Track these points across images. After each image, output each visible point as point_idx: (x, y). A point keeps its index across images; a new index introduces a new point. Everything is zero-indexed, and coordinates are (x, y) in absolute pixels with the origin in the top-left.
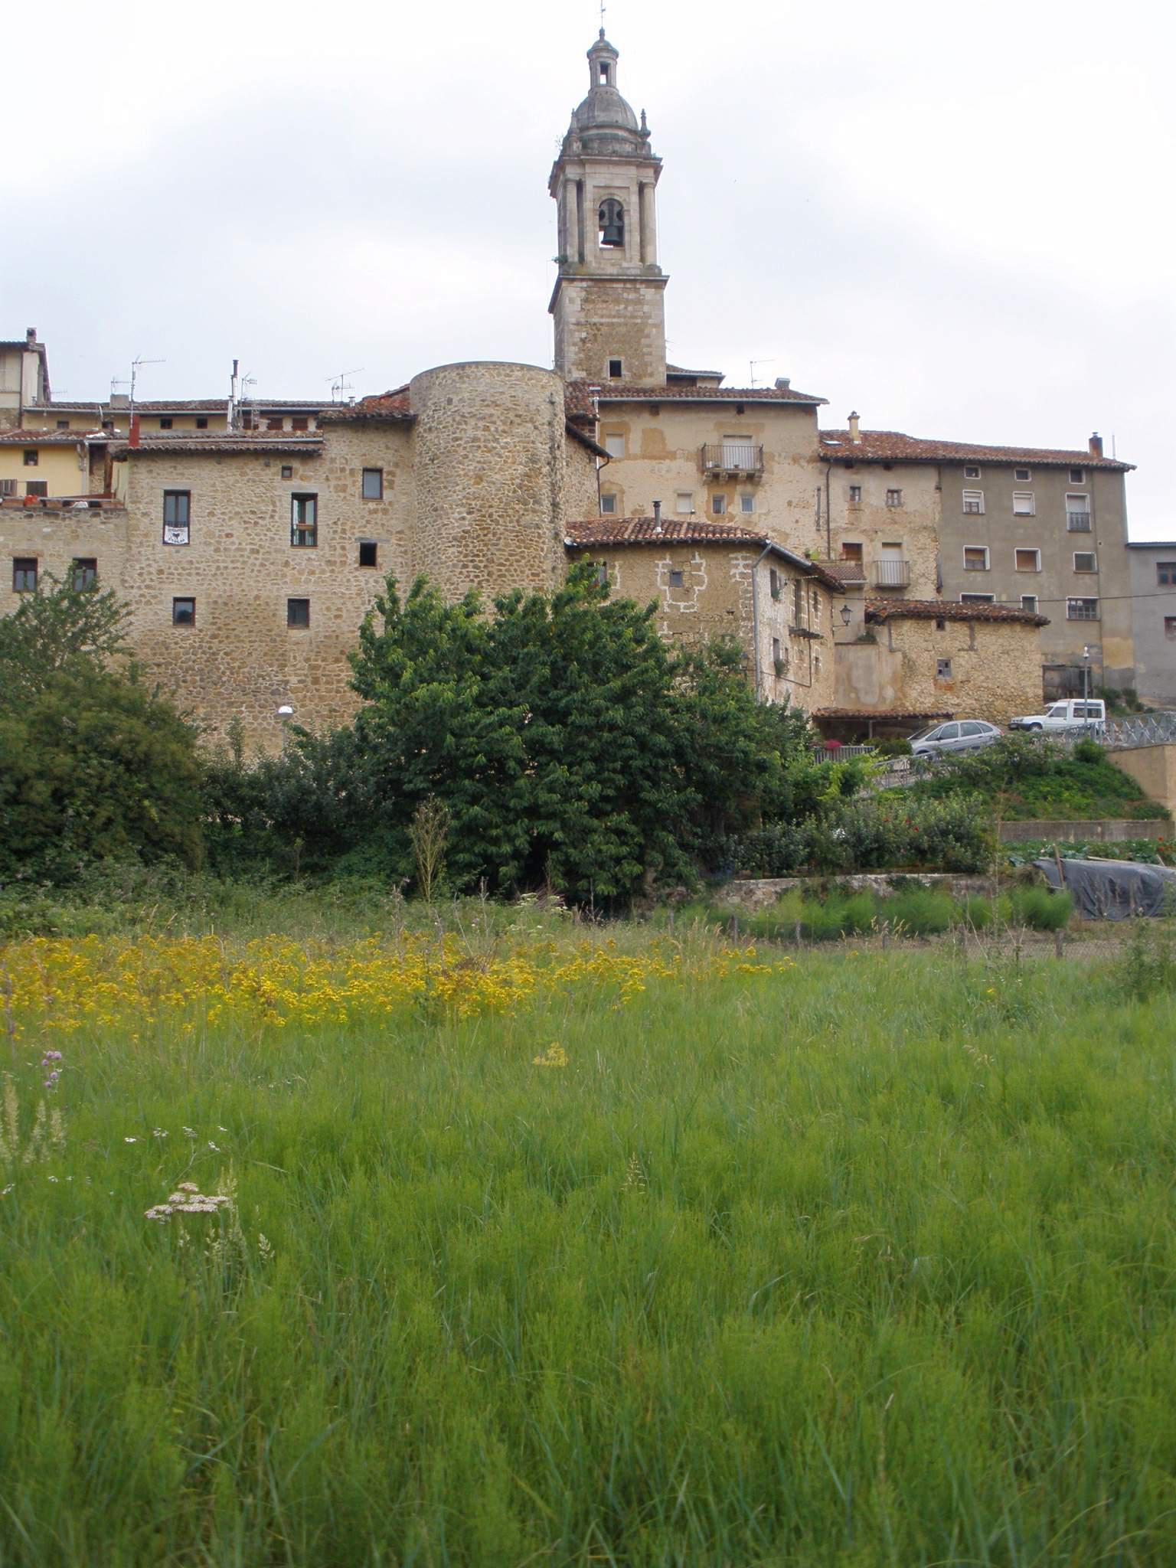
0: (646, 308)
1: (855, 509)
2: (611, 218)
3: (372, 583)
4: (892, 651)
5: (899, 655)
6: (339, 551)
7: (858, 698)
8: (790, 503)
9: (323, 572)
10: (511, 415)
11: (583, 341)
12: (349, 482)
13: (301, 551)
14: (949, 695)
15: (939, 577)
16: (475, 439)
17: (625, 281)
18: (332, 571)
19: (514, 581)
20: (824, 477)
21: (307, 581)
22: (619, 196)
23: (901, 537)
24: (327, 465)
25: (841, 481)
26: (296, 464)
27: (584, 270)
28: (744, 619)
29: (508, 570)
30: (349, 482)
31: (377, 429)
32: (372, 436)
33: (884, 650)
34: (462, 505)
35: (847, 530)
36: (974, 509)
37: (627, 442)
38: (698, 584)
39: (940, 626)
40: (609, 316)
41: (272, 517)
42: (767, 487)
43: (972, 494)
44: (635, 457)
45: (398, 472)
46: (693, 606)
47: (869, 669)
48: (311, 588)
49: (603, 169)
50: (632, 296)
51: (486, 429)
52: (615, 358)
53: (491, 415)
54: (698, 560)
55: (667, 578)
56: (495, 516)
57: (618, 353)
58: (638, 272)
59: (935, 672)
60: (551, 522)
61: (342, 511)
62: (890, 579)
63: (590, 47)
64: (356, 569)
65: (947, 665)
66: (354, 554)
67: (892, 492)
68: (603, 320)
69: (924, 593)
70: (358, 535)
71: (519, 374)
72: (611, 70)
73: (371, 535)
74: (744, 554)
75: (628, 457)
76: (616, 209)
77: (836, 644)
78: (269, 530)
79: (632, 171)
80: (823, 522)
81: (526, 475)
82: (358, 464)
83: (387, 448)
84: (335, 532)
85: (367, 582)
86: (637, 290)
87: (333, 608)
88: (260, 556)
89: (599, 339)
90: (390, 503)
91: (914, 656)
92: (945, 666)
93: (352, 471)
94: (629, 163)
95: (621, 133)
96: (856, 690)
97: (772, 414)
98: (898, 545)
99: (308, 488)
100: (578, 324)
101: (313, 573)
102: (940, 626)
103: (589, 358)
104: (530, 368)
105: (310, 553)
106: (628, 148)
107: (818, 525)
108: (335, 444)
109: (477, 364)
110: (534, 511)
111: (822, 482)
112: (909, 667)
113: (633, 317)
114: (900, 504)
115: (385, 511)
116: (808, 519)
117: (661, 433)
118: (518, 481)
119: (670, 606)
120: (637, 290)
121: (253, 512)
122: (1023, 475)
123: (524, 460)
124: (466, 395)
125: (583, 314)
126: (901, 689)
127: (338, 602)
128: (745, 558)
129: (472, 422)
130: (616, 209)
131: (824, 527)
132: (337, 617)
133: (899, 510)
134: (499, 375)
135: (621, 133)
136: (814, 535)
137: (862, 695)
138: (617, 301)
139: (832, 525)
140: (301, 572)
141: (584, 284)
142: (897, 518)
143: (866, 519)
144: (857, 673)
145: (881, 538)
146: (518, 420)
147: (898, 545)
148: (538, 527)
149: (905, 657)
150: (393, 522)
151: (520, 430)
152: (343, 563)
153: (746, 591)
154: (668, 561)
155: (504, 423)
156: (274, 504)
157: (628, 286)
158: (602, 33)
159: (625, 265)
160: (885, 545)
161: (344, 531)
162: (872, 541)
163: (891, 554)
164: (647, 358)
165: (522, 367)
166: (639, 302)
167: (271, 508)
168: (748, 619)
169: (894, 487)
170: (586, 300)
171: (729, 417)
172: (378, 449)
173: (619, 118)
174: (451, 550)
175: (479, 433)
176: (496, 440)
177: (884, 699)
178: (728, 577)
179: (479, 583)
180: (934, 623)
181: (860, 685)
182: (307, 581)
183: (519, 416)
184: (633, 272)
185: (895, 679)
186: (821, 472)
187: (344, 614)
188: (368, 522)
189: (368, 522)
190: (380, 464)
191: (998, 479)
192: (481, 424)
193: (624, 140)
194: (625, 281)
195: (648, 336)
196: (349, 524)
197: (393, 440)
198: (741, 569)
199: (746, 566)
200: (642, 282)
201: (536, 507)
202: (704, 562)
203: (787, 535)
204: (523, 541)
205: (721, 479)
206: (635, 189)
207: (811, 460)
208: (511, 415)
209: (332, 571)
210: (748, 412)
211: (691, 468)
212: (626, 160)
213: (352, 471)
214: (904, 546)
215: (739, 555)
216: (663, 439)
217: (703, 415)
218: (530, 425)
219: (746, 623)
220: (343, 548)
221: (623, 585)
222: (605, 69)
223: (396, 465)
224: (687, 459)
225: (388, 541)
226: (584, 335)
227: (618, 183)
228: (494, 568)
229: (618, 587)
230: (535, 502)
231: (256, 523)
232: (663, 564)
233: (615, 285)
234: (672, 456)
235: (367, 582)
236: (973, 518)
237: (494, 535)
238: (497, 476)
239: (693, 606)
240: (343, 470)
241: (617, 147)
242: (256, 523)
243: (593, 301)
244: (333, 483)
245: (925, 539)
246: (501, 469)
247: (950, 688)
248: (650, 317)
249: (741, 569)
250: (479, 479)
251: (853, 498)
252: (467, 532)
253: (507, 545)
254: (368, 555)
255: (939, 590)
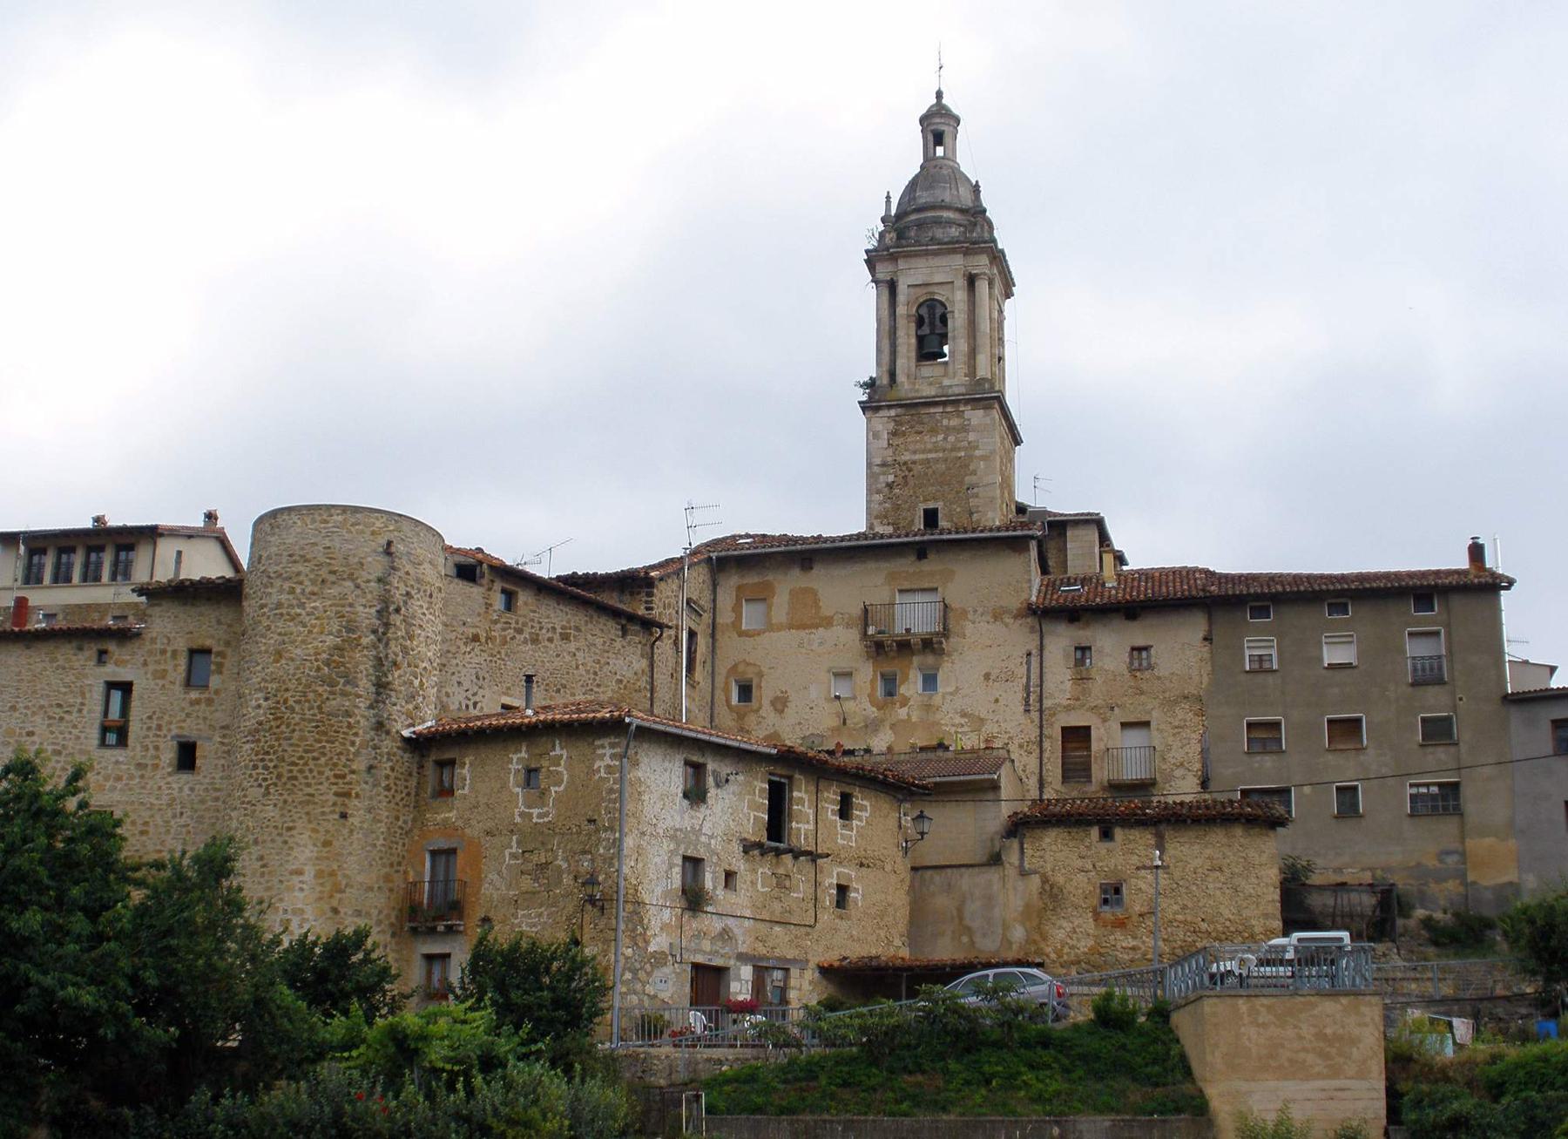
0: (972, 437)
1: (1082, 678)
2: (932, 324)
3: (186, 790)
4: (1023, 873)
5: (1036, 880)
6: (152, 752)
7: (973, 943)
8: (987, 676)
9: (131, 777)
10: (324, 573)
11: (890, 486)
12: (169, 667)
13: (108, 753)
14: (1118, 934)
15: (1205, 765)
16: (279, 605)
17: (944, 404)
18: (142, 777)
19: (308, 785)
20: (1036, 637)
21: (113, 789)
22: (941, 295)
23: (1149, 713)
24: (148, 646)
25: (1061, 640)
26: (112, 647)
27: (894, 394)
28: (606, 830)
29: (301, 771)
30: (169, 667)
31: (209, 599)
32: (203, 609)
33: (1011, 872)
34: (260, 690)
35: (1068, 709)
36: (1266, 665)
37: (770, 608)
38: (556, 785)
39: (1106, 835)
40: (923, 452)
41: (80, 711)
42: (955, 656)
43: (1259, 644)
44: (780, 628)
45: (229, 651)
46: (546, 814)
47: (989, 900)
48: (116, 796)
49: (920, 263)
50: (955, 422)
51: (292, 591)
52: (931, 505)
53: (299, 574)
54: (558, 751)
55: (522, 776)
56: (291, 702)
57: (935, 499)
58: (963, 390)
59: (1095, 901)
60: (371, 707)
61: (161, 702)
62: (1132, 771)
63: (924, 111)
64: (170, 774)
65: (1117, 891)
66: (169, 755)
67: (1140, 649)
68: (917, 457)
69: (1183, 789)
70: (175, 732)
71: (340, 518)
72: (947, 139)
73: (190, 730)
74: (613, 740)
75: (771, 627)
76: (939, 311)
77: (914, 869)
78: (75, 727)
79: (958, 261)
80: (1035, 700)
81: (337, 648)
82: (182, 645)
83: (219, 622)
84: (149, 728)
85: (181, 789)
86: (960, 414)
87: (139, 822)
88: (62, 759)
89: (911, 482)
90: (217, 692)
91: (1060, 880)
92: (1112, 893)
93: (175, 653)
94: (954, 251)
95: (946, 214)
96: (969, 930)
97: (965, 556)
98: (1146, 724)
99: (124, 674)
100: (884, 465)
101: (119, 779)
102: (1106, 835)
103: (897, 508)
104: (356, 510)
105: (119, 755)
106: (954, 232)
107: (1027, 703)
108: (158, 621)
109: (289, 509)
110: (344, 694)
111: (1033, 647)
112: (1052, 896)
113: (954, 449)
114: (1150, 667)
115: (210, 702)
116: (1013, 696)
117: (814, 593)
118: (325, 656)
119: (522, 814)
120: (960, 414)
121: (59, 706)
122: (1261, 612)
123: (335, 628)
124: (274, 549)
125: (890, 452)
126: (1039, 928)
127: (146, 814)
128: (612, 746)
129: (278, 583)
130: (939, 311)
131: (1034, 706)
132: (142, 833)
133: (1147, 674)
134: (314, 521)
135: (946, 214)
136: (1023, 719)
137: (978, 939)
138: (934, 431)
139: (1047, 703)
140: (107, 778)
141: (893, 413)
142: (1144, 686)
143: (1098, 690)
144: (973, 907)
145: (1119, 715)
146: (332, 578)
147: (1146, 724)
148: (348, 714)
149: (1045, 880)
150: (217, 715)
151: (333, 591)
152: (156, 767)
153: (611, 791)
154: (524, 755)
155: (313, 582)
156: (83, 694)
157: (949, 409)
158: (939, 95)
159: (946, 382)
160: (1124, 725)
161: (159, 727)
162: (1105, 720)
163: (1135, 738)
164: (973, 502)
165: (345, 509)
166: (964, 429)
167: (79, 700)
168: (612, 829)
169: (1140, 642)
170: (894, 434)
171: (906, 564)
172: (204, 626)
173: (947, 196)
174: (247, 746)
175: (284, 597)
176: (302, 606)
177: (1011, 943)
178: (592, 772)
179: (267, 788)
180: (1095, 832)
181: (976, 924)
182: (113, 789)
183: (334, 572)
184: (956, 390)
185: (1027, 913)
186: (1032, 630)
187: (151, 830)
188: (188, 715)
189: (188, 715)
190: (208, 643)
191: (1299, 619)
192: (286, 586)
193: (950, 223)
194: (944, 404)
195: (974, 473)
196: (166, 718)
197: (225, 613)
198: (608, 761)
199: (613, 757)
200: (967, 402)
201: (349, 688)
202: (565, 753)
203: (982, 720)
204: (325, 733)
205: (891, 650)
206: (961, 282)
207: (1018, 616)
208: (324, 573)
209: (142, 777)
210: (932, 556)
211: (853, 635)
212: (951, 247)
213: (175, 653)
214: (1153, 725)
215: (606, 741)
216: (816, 602)
217: (871, 565)
218: (348, 584)
219: (608, 834)
220: (157, 748)
221: (472, 788)
222: (939, 139)
223: (228, 644)
224: (848, 626)
225: (209, 739)
226: (891, 478)
227: (937, 279)
228: (284, 768)
229: (466, 791)
230: (347, 683)
231: (61, 719)
232: (518, 758)
233: (932, 410)
234: (828, 622)
235: (181, 789)
236: (1260, 678)
237: (288, 726)
238: (298, 651)
239: (546, 814)
240: (163, 652)
241: (939, 233)
242: (61, 719)
243: (904, 434)
244: (151, 668)
245: (1183, 713)
246: (303, 642)
247: (1121, 924)
248: (977, 448)
249: (608, 761)
250: (279, 655)
251: (1080, 663)
252: (260, 723)
253: (302, 739)
254: (187, 756)
255: (1204, 784)
